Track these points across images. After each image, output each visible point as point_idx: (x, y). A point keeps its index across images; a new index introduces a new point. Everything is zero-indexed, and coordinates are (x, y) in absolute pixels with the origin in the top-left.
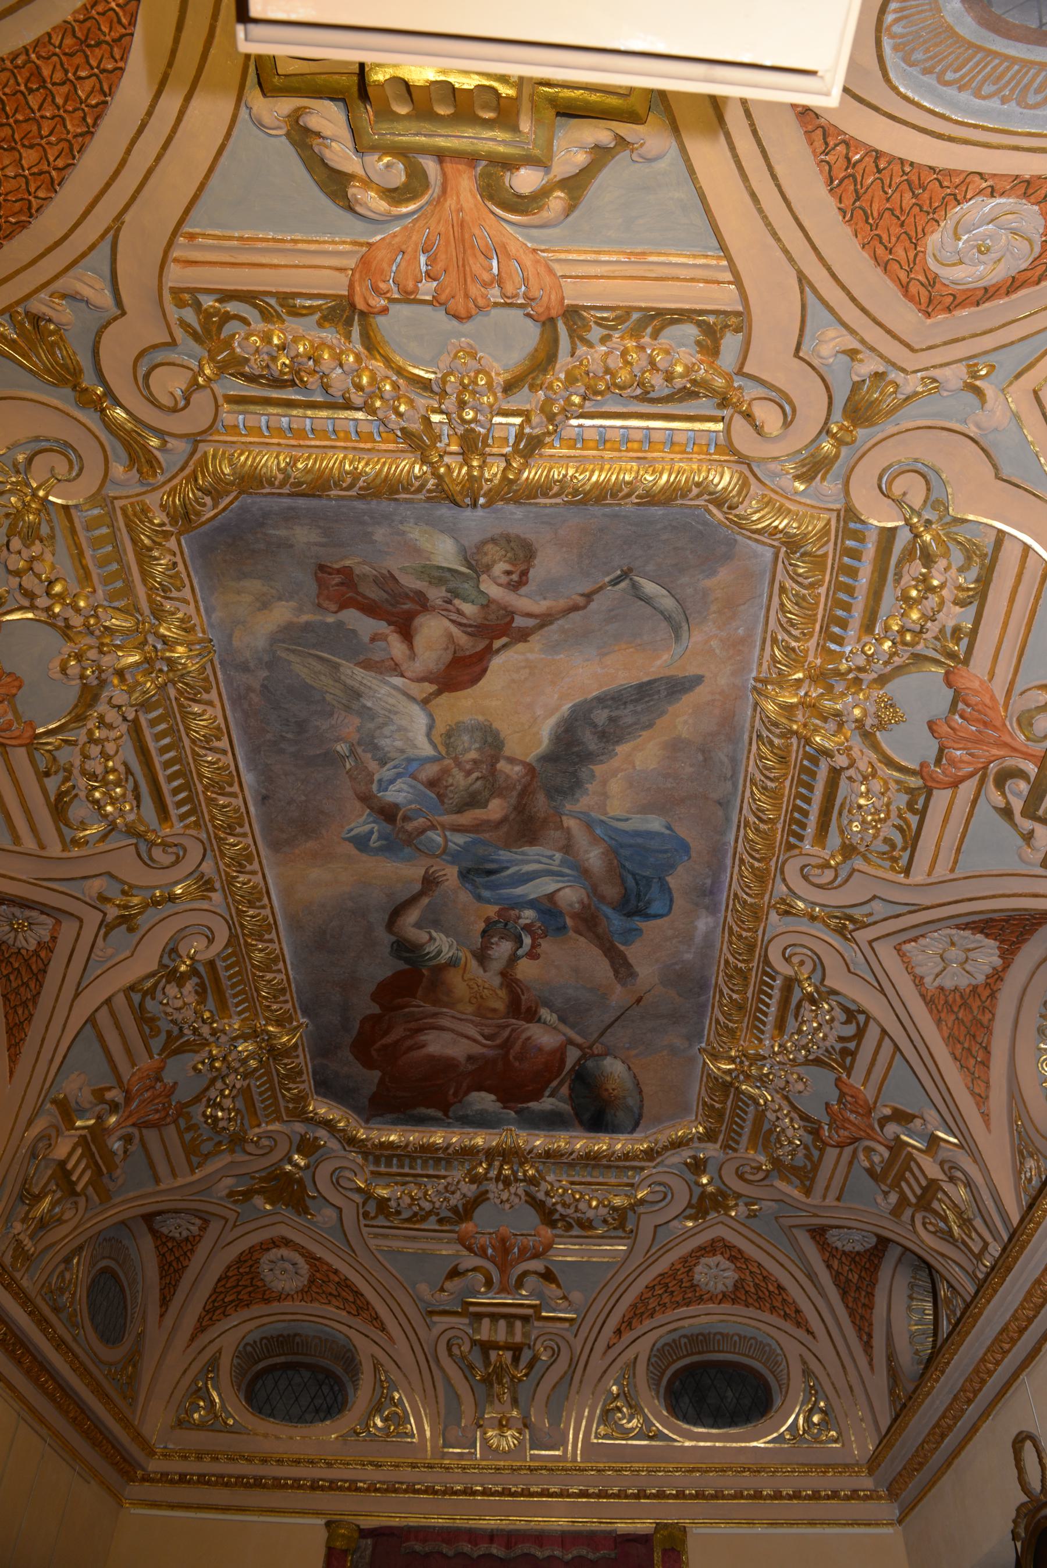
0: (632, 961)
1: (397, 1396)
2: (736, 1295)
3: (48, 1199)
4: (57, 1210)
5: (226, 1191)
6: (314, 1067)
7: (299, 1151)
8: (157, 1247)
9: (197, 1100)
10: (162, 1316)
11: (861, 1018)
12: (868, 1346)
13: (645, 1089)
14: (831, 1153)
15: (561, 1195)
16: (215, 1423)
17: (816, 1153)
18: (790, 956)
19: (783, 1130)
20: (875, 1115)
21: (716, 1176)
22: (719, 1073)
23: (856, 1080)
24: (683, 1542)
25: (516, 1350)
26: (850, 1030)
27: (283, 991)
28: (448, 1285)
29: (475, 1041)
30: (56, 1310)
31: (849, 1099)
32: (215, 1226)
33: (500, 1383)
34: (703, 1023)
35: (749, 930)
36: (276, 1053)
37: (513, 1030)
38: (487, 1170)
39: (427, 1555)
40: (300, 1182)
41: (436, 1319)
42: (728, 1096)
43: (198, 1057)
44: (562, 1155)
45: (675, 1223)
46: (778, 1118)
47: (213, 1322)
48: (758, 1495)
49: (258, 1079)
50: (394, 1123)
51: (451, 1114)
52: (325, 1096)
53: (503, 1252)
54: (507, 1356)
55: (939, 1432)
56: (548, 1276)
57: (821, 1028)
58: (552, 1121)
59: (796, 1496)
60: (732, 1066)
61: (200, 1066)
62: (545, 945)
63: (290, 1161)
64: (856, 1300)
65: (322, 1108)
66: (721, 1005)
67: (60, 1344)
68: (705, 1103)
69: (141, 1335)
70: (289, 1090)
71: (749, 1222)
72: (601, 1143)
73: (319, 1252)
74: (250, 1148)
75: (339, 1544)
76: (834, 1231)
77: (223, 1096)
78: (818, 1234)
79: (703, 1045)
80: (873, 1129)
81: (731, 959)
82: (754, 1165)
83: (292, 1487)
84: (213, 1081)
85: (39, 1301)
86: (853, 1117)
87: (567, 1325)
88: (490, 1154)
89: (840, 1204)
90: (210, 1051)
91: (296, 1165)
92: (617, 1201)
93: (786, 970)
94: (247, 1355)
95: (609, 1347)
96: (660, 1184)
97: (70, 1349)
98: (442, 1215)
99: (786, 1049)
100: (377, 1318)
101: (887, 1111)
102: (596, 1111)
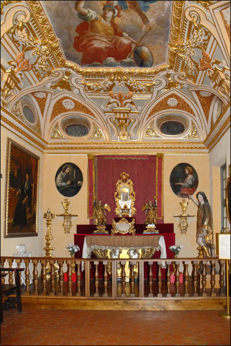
0: (147, 17)
1: (99, 130)
2: (177, 107)
3: (6, 91)
4: (9, 93)
5: (50, 86)
6: (64, 52)
7: (66, 75)
8: (37, 101)
9: (36, 63)
10: (42, 116)
11: (209, 34)
12: (207, 118)
13: (154, 55)
14: (201, 72)
15: (134, 84)
16: (60, 137)
17: (197, 72)
18: (191, 15)
19: (189, 66)
20: (212, 62)
21: (173, 78)
22: (172, 50)
23: (207, 52)
24: (163, 156)
25: (126, 120)
26: (206, 38)
27: (50, 31)
28: (109, 106)
29: (106, 43)
30: (17, 116)
31: (205, 57)
32: (49, 95)
33: (122, 127)
34: (168, 36)
35: (179, 6)
36: (54, 49)
37: (116, 39)
38: (114, 78)
39: (109, 160)
40: (68, 83)
41: (106, 113)
42: (175, 57)
43: (32, 51)
44: (133, 73)
45: (163, 90)
46: (188, 63)
47: (55, 117)
48: (179, 148)
49: (50, 56)
50: (88, 66)
51: (103, 63)
52: (69, 60)
53: (120, 98)
54: (124, 121)
55: (217, 135)
56: (132, 103)
57: (199, 37)
58: (130, 65)
59: (188, 148)
60: (176, 48)
61: (34, 54)
62: (122, 13)
63: (64, 78)
64: (206, 108)
65: (69, 63)
66: (173, 30)
67: (20, 122)
68: (169, 59)
69: (39, 121)
70: (59, 59)
71: (182, 90)
72: (143, 70)
73: (76, 100)
74: (53, 75)
75: (90, 158)
76: (201, 92)
77: (42, 62)
78: (198, 92)
79: (169, 42)
80: (210, 66)
81: (175, 16)
82: (182, 75)
83: (79, 149)
84: (38, 58)
85: (12, 113)
86: (206, 62)
87: (137, 114)
88: (115, 74)
89: (203, 85)
90: (35, 49)
91: (66, 79)
92: (148, 85)
93: (190, 19)
94: (64, 123)
95: (147, 119)
96: (158, 80)
97: (22, 123)
98: (104, 89)
99: (190, 43)
100: (92, 114)
101: (214, 61)
102: (141, 62)
